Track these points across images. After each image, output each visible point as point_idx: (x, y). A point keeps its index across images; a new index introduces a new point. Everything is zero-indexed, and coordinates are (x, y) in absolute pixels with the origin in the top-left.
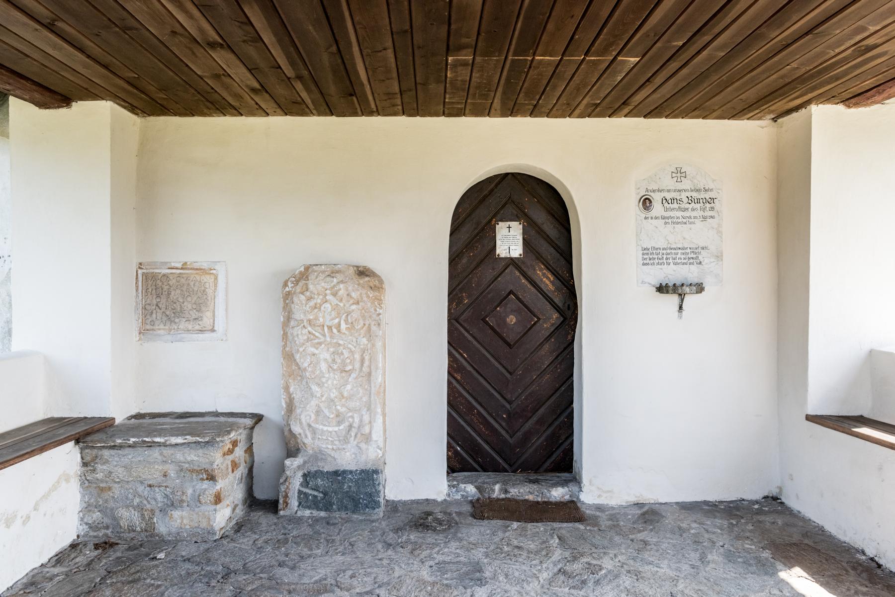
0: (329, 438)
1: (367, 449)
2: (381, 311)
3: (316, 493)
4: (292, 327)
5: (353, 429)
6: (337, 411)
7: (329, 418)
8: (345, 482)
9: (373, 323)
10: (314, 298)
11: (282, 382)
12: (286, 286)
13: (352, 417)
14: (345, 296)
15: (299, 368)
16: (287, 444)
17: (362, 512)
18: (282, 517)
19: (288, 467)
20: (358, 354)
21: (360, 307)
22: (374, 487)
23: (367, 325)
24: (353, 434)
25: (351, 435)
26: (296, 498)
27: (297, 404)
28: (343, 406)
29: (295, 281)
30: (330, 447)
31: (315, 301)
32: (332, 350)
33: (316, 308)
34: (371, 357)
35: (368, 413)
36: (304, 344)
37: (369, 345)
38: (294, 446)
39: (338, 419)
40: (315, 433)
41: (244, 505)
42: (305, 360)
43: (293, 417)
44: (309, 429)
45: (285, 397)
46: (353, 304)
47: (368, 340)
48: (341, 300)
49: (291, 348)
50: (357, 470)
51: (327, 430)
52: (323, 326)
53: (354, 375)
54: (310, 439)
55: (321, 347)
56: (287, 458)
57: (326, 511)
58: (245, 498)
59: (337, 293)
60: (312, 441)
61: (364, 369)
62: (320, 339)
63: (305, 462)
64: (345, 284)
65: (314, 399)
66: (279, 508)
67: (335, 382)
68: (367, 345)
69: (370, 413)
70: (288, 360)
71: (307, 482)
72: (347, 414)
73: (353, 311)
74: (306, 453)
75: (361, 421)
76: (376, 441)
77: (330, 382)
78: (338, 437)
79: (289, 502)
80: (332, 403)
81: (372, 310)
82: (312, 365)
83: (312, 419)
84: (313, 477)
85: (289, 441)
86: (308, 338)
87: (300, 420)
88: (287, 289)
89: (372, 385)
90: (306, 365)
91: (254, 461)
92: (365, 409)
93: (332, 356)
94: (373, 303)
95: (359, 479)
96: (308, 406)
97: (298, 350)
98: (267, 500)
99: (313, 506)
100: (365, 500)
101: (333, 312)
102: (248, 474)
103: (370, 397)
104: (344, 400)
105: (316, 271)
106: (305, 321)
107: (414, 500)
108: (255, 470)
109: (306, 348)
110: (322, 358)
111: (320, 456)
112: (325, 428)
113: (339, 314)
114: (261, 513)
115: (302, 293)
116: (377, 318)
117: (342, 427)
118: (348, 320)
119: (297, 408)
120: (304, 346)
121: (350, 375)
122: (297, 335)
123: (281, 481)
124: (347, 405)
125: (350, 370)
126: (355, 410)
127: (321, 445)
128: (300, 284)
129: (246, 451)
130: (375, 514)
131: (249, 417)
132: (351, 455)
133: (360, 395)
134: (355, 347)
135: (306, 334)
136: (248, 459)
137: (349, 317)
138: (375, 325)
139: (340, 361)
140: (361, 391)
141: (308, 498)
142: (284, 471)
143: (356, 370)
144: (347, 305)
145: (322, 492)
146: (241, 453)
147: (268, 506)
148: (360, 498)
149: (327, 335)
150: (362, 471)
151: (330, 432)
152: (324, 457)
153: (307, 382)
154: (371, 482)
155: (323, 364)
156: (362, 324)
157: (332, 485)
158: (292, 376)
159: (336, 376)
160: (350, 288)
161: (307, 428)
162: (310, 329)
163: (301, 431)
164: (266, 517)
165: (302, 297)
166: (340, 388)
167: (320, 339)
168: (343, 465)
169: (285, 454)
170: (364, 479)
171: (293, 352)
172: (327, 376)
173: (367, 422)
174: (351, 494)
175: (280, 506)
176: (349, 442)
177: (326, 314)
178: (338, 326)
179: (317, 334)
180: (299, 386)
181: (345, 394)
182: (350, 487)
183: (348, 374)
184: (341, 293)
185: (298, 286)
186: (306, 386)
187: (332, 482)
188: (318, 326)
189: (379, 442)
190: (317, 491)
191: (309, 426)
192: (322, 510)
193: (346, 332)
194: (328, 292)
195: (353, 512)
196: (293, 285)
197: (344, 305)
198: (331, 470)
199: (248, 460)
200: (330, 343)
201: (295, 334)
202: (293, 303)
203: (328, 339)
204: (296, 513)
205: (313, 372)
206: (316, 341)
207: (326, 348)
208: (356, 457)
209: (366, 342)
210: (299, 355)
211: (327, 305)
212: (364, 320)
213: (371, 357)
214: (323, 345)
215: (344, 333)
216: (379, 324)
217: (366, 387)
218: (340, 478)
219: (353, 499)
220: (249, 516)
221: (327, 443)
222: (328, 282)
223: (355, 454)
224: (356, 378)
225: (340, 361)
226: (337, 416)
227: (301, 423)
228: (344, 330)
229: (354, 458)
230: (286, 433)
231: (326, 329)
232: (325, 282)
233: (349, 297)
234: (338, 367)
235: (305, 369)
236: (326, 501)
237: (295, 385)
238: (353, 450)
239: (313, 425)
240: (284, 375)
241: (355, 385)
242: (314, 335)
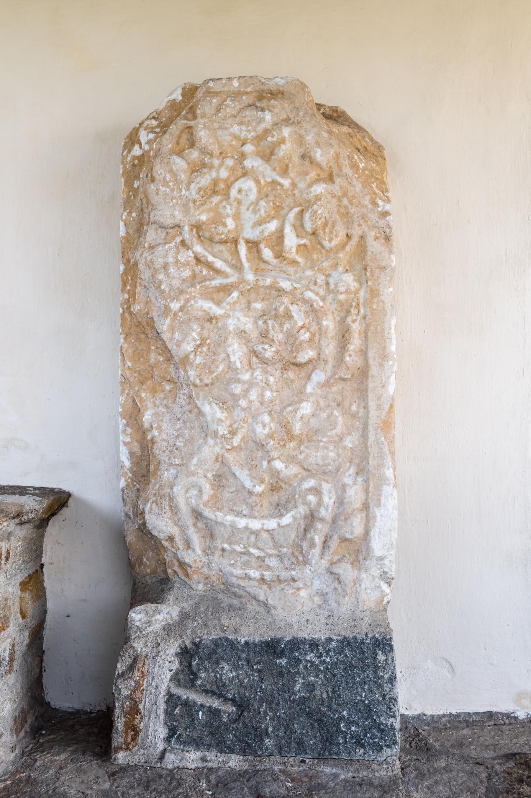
0: (252, 550)
1: (357, 581)
2: (388, 207)
3: (216, 704)
4: (152, 248)
5: (319, 526)
6: (275, 473)
7: (251, 493)
8: (298, 673)
9: (373, 234)
10: (211, 167)
11: (122, 399)
12: (133, 145)
13: (317, 491)
14: (296, 159)
15: (170, 359)
16: (131, 565)
17: (344, 756)
18: (124, 769)
19: (139, 629)
20: (330, 317)
21: (336, 189)
22: (379, 687)
23: (355, 240)
24: (318, 540)
25: (312, 540)
26: (162, 716)
27: (163, 457)
28: (290, 460)
29: (158, 126)
30: (254, 574)
31: (214, 174)
32: (258, 306)
33: (215, 192)
34: (368, 326)
35: (360, 480)
36: (182, 292)
37: (362, 293)
38: (154, 572)
39: (275, 498)
40: (212, 536)
41: (17, 732)
42: (185, 335)
43: (151, 492)
44: (195, 525)
45: (128, 440)
46: (318, 180)
47: (359, 280)
48: (285, 171)
49: (148, 302)
50: (330, 640)
51: (246, 528)
52: (236, 242)
53: (319, 376)
54: (199, 552)
55: (229, 299)
56: (131, 608)
57: (243, 752)
58: (23, 711)
59: (272, 153)
60: (204, 559)
61: (348, 359)
62: (226, 276)
63: (184, 617)
64: (296, 128)
65: (211, 442)
66: (114, 744)
67: (268, 394)
68: (356, 293)
69: (366, 481)
70: (138, 339)
71: (192, 673)
72: (300, 485)
73: (318, 198)
74: (186, 592)
75: (341, 502)
76: (381, 559)
77: (253, 395)
78: (277, 546)
79: (142, 726)
80: (260, 454)
81: (367, 201)
82: (205, 349)
83: (205, 497)
84: (209, 659)
85: (140, 559)
86: (194, 276)
87: (171, 499)
88: (137, 151)
89: (372, 404)
90: (188, 347)
91: (45, 612)
92: (352, 471)
93: (260, 323)
94: (366, 184)
95: (335, 665)
96: (195, 461)
97: (167, 307)
98: (78, 712)
99: (207, 740)
100: (353, 723)
101: (263, 203)
102: (30, 646)
103: (365, 436)
104: (292, 445)
105: (217, 94)
106: (186, 228)
107: (458, 715)
108: (47, 633)
109: (187, 301)
110: (231, 328)
111: (225, 600)
112: (242, 523)
113: (278, 208)
114: (63, 756)
115: (180, 154)
116: (381, 223)
117: (287, 520)
118: (302, 226)
119: (163, 467)
120: (183, 298)
121: (309, 378)
122: (165, 267)
123: (121, 667)
124: (301, 457)
125: (310, 361)
126: (325, 473)
127: (228, 569)
128: (174, 129)
129: (24, 586)
130: (380, 764)
131: (33, 495)
132: (311, 597)
133: (338, 430)
134: (323, 299)
135: (188, 264)
136: (30, 607)
137: (307, 215)
138: (376, 238)
139: (281, 336)
140: (340, 420)
141: (193, 718)
142: (127, 640)
143: (326, 362)
144: (302, 185)
145: (233, 701)
146: (10, 589)
147: (82, 731)
148: (341, 718)
149: (246, 265)
150: (345, 642)
151: (256, 533)
152: (235, 602)
153: (190, 397)
154: (370, 672)
155: (236, 346)
156: (342, 233)
157: (262, 680)
158: (149, 383)
159: (272, 380)
160: (310, 138)
161: (189, 522)
162: (198, 249)
163: (174, 531)
164: (79, 770)
165: (179, 163)
166: (282, 411)
167: (226, 276)
168: (290, 626)
169: (124, 592)
170: (352, 666)
171: (154, 314)
172: (246, 377)
173: (358, 505)
174: (313, 705)
175: (118, 739)
176: (306, 562)
177: (243, 208)
178: (280, 236)
179: (219, 264)
180: (166, 406)
181: (297, 428)
182: (311, 687)
183: (303, 374)
184: (284, 150)
185: (167, 136)
186: (187, 408)
187: (260, 671)
188: (222, 242)
189: (386, 562)
190: (220, 696)
191: (197, 515)
192: (232, 751)
193: (299, 259)
194: (249, 148)
195: (321, 757)
196: (151, 136)
197: (294, 185)
198: (257, 639)
199: (30, 610)
200: (255, 288)
201: (159, 262)
202: (153, 180)
203: (250, 277)
204: (162, 757)
205: (207, 368)
206: (217, 282)
207: (243, 301)
208: (326, 601)
209: (354, 285)
210: (168, 321)
211: (248, 184)
212: (349, 223)
213: (368, 326)
214: (235, 294)
215: (294, 262)
216: (388, 239)
217: (354, 408)
218: (283, 661)
219: (320, 721)
220: (30, 766)
221: (246, 564)
222: (248, 124)
223: (323, 595)
224: (326, 384)
225: (280, 337)
226: (274, 489)
227: (174, 509)
228: (294, 250)
229: (320, 606)
230: (131, 538)
231: (243, 249)
232: (241, 123)
233: (307, 163)
234: (277, 352)
235: (185, 361)
236: (245, 725)
237: (155, 405)
238: (317, 584)
239: (207, 512)
240: (125, 381)
241: (322, 403)
242: (210, 266)
